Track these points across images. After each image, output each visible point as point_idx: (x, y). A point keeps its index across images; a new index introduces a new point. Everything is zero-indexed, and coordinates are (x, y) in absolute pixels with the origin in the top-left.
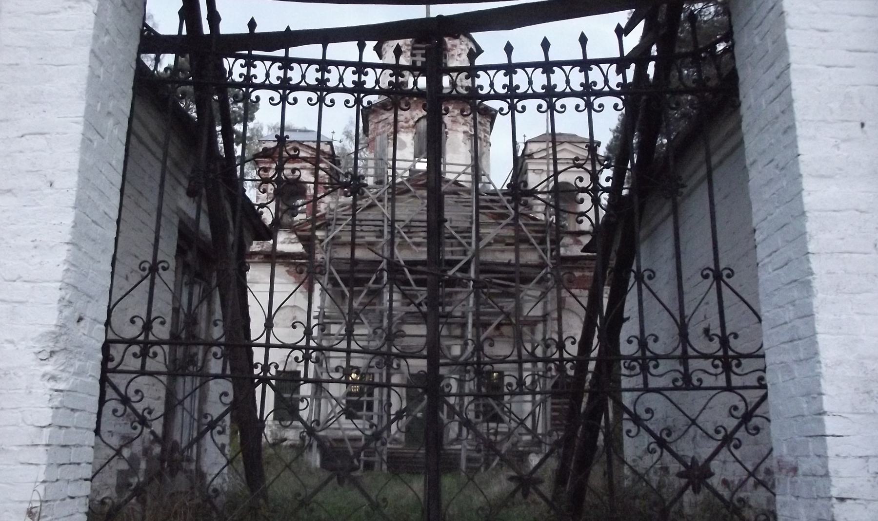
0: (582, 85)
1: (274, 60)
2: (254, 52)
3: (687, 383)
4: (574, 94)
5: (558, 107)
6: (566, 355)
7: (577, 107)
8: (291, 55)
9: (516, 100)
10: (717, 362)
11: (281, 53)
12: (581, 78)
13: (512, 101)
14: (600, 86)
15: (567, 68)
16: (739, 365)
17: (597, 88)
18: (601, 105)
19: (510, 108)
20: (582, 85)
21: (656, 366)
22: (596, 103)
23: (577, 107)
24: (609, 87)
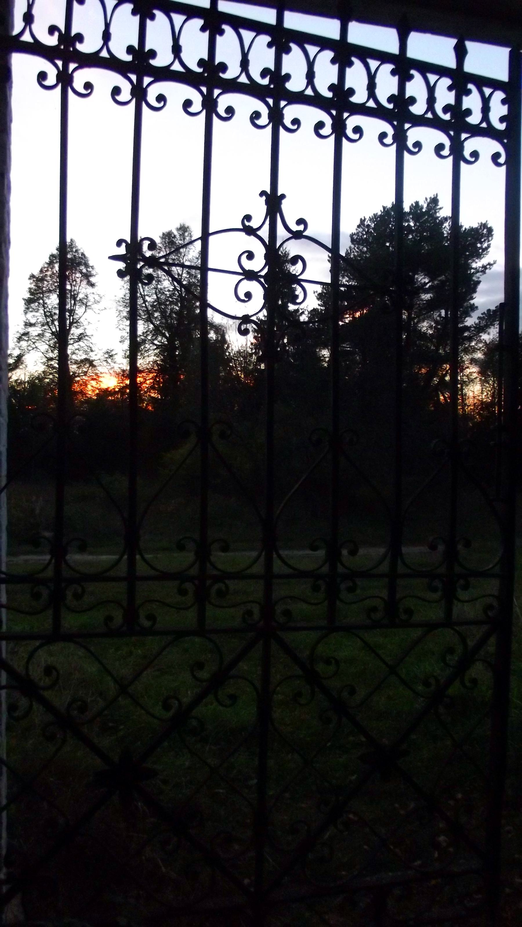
0: (130, 50)
1: (258, 28)
2: (294, 21)
3: (393, 615)
4: (112, 64)
5: (151, 98)
6: (194, 571)
7: (187, 104)
8: (412, 53)
9: (72, 66)
10: (147, 624)
11: (267, 15)
12: (450, 98)
13: (66, 66)
14: (233, 72)
15: (247, 35)
16: (466, 587)
17: (228, 75)
18: (358, 130)
19: (205, 104)
20: (130, 50)
21: (351, 590)
22: (153, 92)
23: (187, 104)
24: (249, 77)
